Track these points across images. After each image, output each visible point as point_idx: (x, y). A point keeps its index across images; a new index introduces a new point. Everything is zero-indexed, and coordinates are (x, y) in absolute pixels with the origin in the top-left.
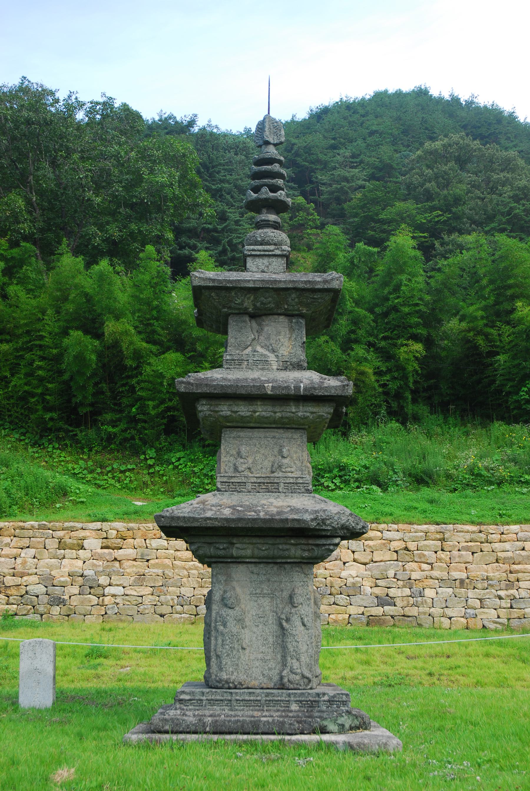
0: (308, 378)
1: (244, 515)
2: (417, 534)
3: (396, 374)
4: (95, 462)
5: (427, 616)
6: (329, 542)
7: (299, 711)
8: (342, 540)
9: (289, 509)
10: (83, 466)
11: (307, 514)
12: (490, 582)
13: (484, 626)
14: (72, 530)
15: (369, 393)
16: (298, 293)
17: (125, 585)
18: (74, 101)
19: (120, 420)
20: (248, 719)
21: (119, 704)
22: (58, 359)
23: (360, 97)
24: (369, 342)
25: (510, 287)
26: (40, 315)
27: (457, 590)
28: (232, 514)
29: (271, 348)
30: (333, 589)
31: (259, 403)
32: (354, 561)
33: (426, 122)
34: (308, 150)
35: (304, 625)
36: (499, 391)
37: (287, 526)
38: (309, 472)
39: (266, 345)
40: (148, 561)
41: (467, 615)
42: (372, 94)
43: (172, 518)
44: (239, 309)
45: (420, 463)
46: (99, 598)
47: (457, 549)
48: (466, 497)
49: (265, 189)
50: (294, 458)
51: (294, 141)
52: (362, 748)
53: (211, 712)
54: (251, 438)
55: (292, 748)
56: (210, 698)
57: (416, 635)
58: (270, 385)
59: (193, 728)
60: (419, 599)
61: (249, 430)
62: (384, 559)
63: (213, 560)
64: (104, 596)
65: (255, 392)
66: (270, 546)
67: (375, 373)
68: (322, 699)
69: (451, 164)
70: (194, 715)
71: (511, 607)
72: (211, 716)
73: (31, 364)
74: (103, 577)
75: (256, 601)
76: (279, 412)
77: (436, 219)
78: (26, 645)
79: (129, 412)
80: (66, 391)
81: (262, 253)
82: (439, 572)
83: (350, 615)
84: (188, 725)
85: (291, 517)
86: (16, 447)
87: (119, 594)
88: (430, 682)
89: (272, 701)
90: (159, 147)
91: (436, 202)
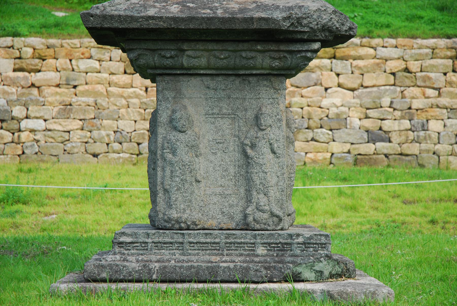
2: (422, 51)
5: (431, 154)
6: (305, 47)
7: (267, 255)
8: (322, 46)
9: (254, 5)
17: (46, 117)
20: (203, 265)
21: (44, 253)
28: (181, 11)
32: (339, 86)
35: (273, 152)
37: (252, 27)
40: (75, 87)
43: (104, 17)
46: (13, 134)
52: (344, 298)
53: (159, 257)
55: (258, 298)
56: (156, 240)
59: (136, 276)
60: (422, 133)
62: (378, 84)
63: (158, 72)
64: (20, 130)
66: (231, 54)
68: (296, 241)
70: (138, 261)
72: (158, 261)
74: (18, 107)
75: (213, 123)
82: (448, 100)
83: (333, 154)
84: (131, 272)
85: (257, 15)
87: (40, 128)
89: (234, 243)
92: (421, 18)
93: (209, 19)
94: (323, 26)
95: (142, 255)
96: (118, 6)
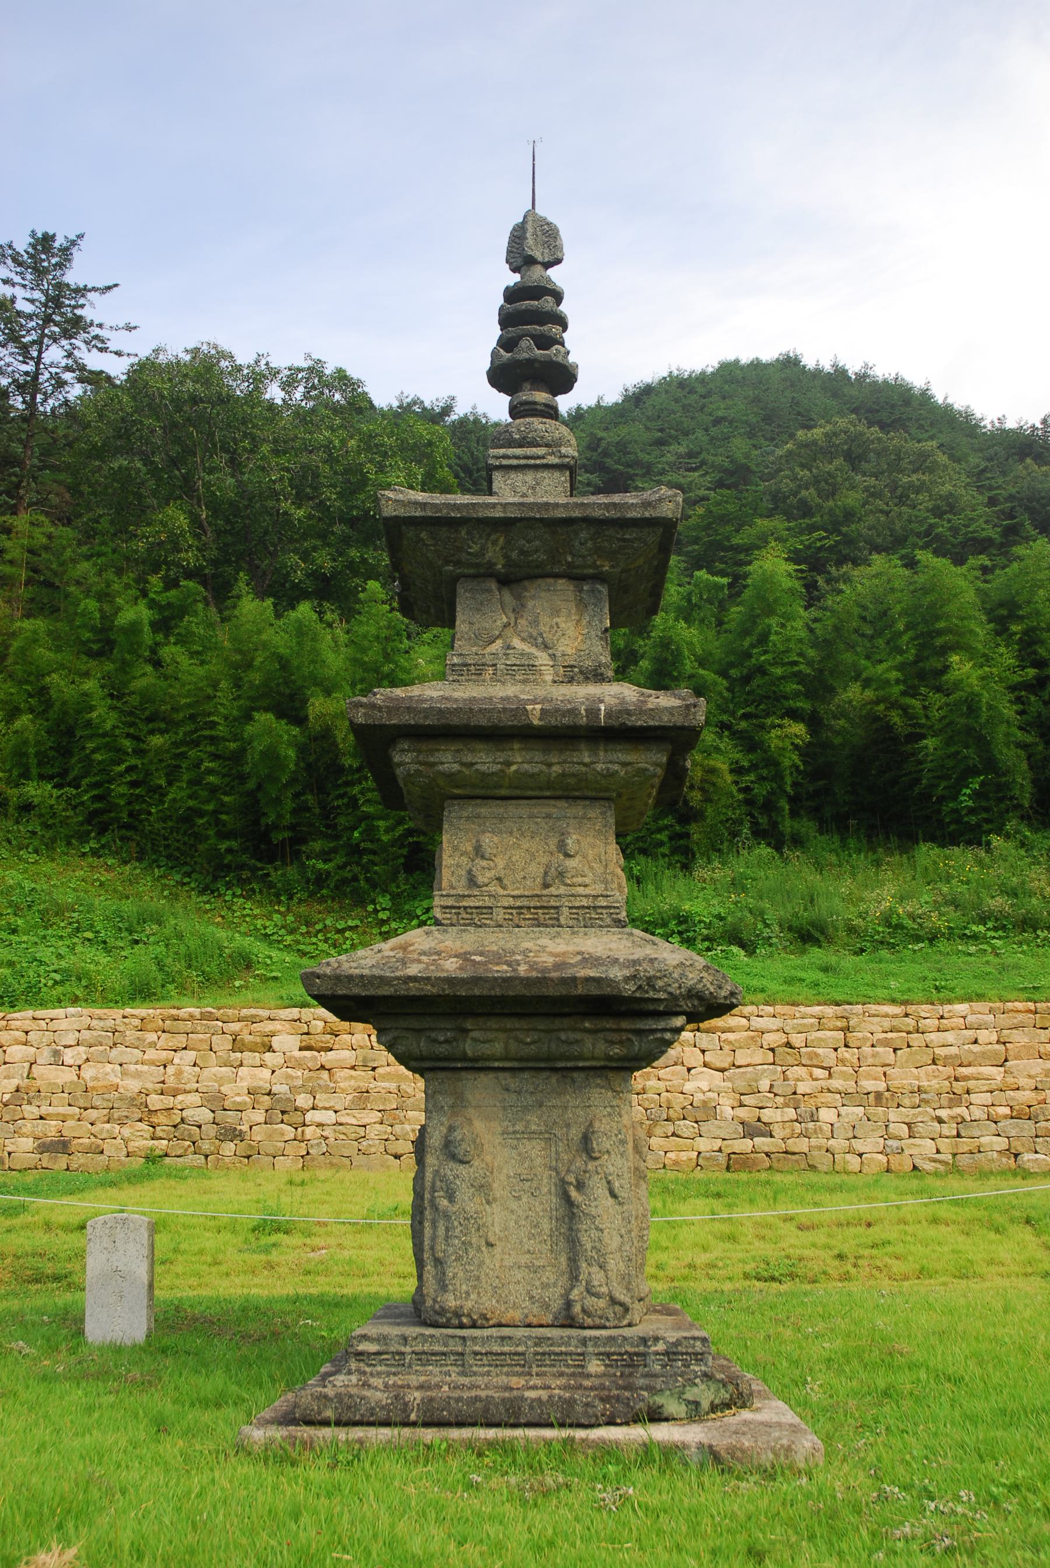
0: (616, 695)
1: (486, 970)
2: (805, 1021)
3: (765, 772)
4: (298, 917)
5: (823, 1152)
6: (661, 1025)
7: (604, 1375)
8: (689, 1022)
9: (579, 957)
10: (279, 923)
11: (617, 968)
12: (923, 1096)
13: (915, 1168)
14: (254, 1020)
15: (723, 802)
16: (593, 530)
17: (337, 1108)
18: (263, 367)
19: (334, 850)
22: (237, 757)
23: (698, 369)
24: (722, 722)
25: (939, 633)
26: (210, 691)
27: (872, 1110)
28: (461, 968)
29: (540, 640)
30: (671, 1111)
31: (516, 746)
33: (798, 404)
34: (622, 447)
35: (613, 1195)
36: (926, 796)
38: (620, 886)
39: (531, 636)
40: (374, 1069)
41: (888, 1150)
42: (717, 366)
43: (338, 978)
44: (477, 566)
45: (805, 910)
47: (869, 1044)
48: (881, 961)
49: (526, 342)
50: (590, 858)
51: (601, 434)
52: (738, 1459)
53: (422, 1379)
54: (502, 819)
56: (419, 1348)
57: (811, 1187)
58: (538, 707)
59: (382, 1415)
60: (811, 1125)
61: (498, 802)
65: (507, 721)
67: (732, 771)
68: (653, 1349)
69: (839, 461)
71: (959, 1136)
72: (420, 1387)
73: (198, 766)
74: (303, 1095)
75: (516, 1148)
76: (557, 764)
77: (818, 544)
78: (99, 1226)
79: (349, 839)
80: (252, 807)
81: (523, 462)
82: (841, 1082)
84: (373, 1409)
85: (582, 973)
86: (177, 895)
88: (841, 1271)
90: (392, 432)
91: (817, 519)
92: (802, 980)
93: (506, 980)
94: (690, 991)
95: (394, 1374)
96: (362, 962)
